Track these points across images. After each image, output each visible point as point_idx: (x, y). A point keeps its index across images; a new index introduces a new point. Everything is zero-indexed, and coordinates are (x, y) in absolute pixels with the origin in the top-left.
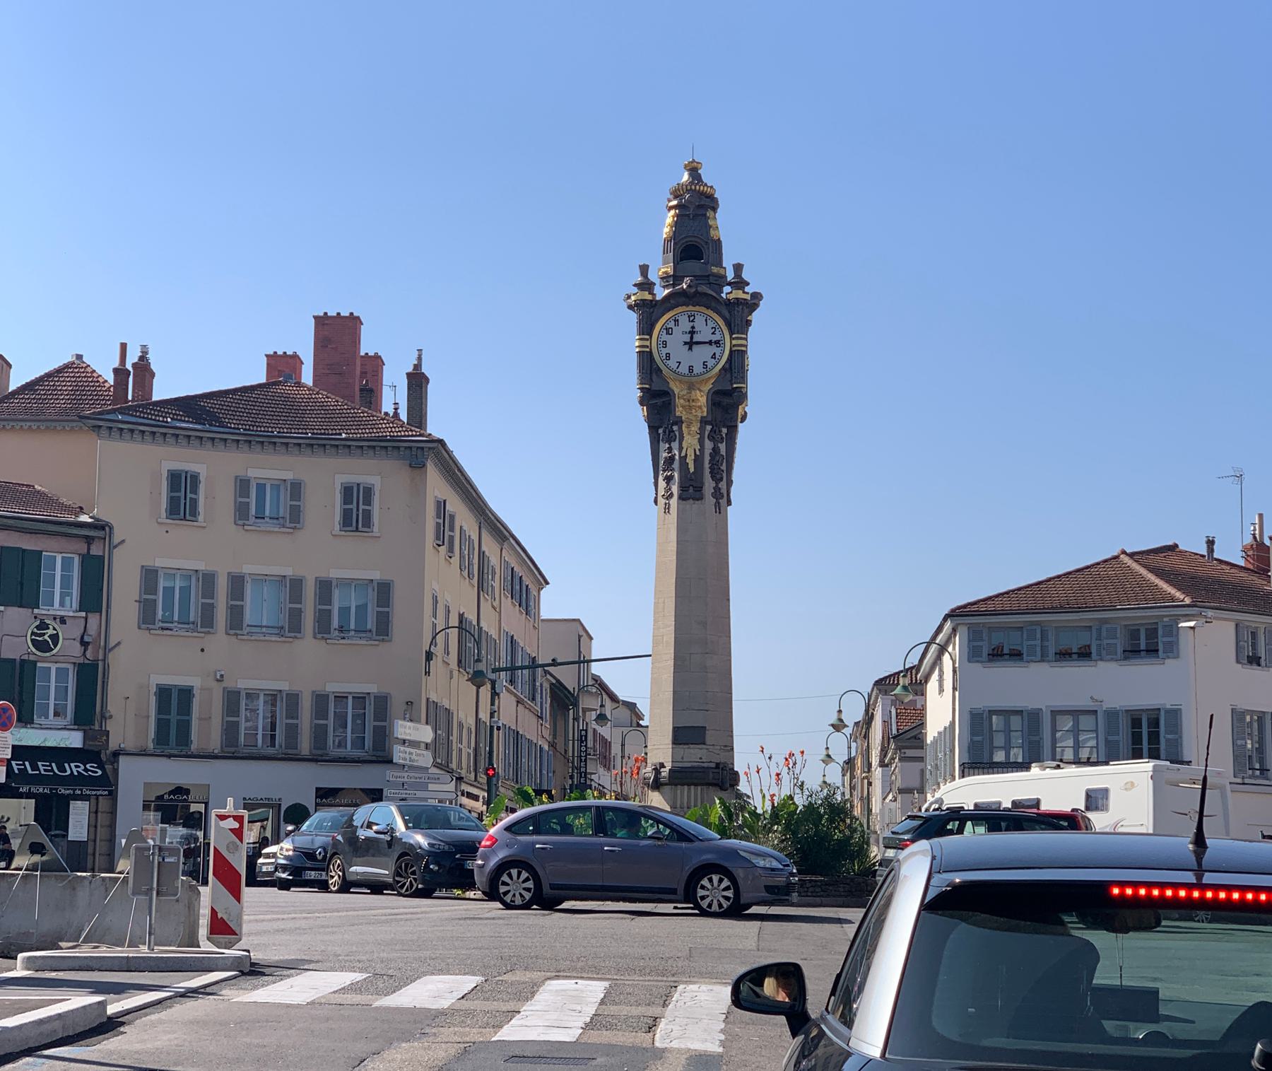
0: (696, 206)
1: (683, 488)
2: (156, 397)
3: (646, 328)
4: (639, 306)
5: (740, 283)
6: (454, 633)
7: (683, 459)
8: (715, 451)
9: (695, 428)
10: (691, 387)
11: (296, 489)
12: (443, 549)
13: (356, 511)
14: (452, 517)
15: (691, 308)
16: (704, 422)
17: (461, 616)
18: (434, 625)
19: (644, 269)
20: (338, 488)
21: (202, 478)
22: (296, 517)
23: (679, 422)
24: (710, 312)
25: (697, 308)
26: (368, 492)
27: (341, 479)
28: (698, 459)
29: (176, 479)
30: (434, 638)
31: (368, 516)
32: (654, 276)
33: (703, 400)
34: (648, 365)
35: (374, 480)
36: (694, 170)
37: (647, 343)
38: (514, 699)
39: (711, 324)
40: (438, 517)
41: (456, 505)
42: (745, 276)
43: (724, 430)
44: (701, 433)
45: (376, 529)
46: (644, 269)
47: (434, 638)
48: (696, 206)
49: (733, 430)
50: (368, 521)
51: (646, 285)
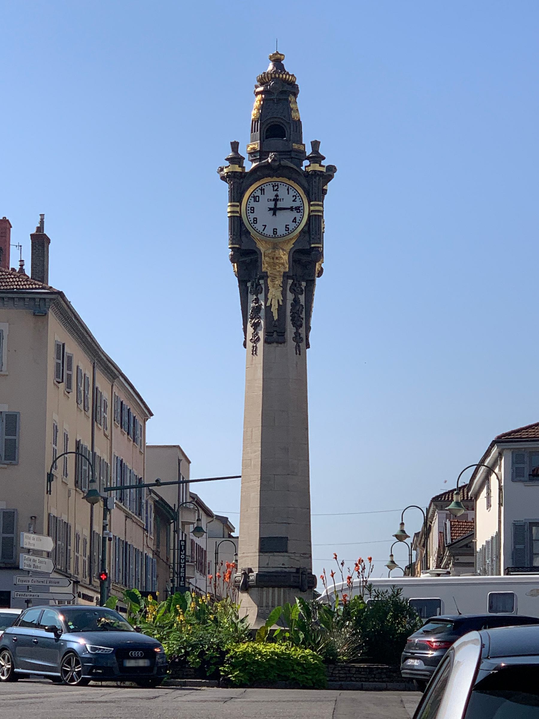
0: (279, 91)
3: (236, 196)
5: (317, 158)
6: (71, 458)
8: (296, 301)
9: (279, 282)
10: (275, 247)
12: (62, 386)
14: (70, 359)
15: (275, 179)
16: (286, 276)
17: (78, 443)
18: (55, 451)
19: (235, 146)
21: (5, 334)
23: (265, 276)
24: (291, 183)
25: (280, 179)
28: (281, 309)
32: (243, 152)
33: (285, 258)
34: (239, 229)
36: (277, 61)
37: (238, 209)
38: (123, 515)
39: (292, 193)
40: (58, 358)
41: (73, 348)
43: (304, 284)
46: (235, 146)
48: (279, 91)
49: (311, 283)
51: (236, 160)
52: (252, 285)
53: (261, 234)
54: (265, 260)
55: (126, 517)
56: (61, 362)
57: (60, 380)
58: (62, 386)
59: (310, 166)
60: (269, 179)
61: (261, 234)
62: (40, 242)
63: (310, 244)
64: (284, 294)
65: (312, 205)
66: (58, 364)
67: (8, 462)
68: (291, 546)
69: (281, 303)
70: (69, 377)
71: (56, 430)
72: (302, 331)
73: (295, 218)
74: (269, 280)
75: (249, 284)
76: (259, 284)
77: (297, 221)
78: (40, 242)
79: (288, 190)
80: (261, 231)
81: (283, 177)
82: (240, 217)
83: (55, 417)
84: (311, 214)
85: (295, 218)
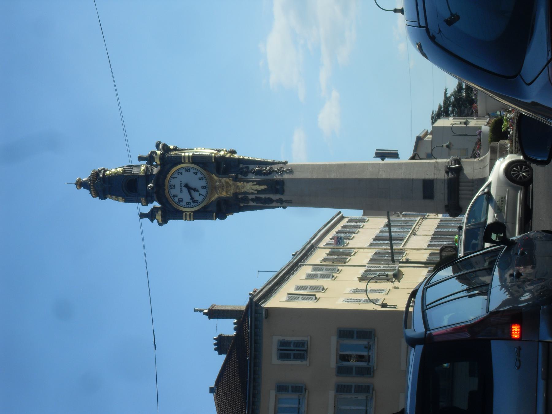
0: (104, 186)
1: (277, 192)
2: (233, 333)
3: (178, 215)
4: (164, 221)
5: (150, 159)
6: (373, 285)
7: (259, 192)
8: (253, 200)
9: (240, 184)
10: (215, 188)
11: (282, 388)
12: (318, 294)
13: (294, 351)
14: (299, 288)
15: (166, 187)
16: (235, 179)
17: (362, 279)
18: (365, 301)
19: (142, 216)
20: (280, 362)
21: (281, 338)
22: (298, 389)
23: (236, 194)
24: (169, 176)
25: (166, 183)
26: (283, 344)
27: (275, 360)
28: (259, 183)
29: (283, 356)
30: (371, 301)
31: (297, 344)
32: (146, 209)
33: (224, 180)
34: (203, 214)
35: (276, 339)
36: (80, 184)
37: (187, 161)
38: (413, 238)
39: (176, 175)
40: (298, 299)
41: (289, 286)
42: (146, 154)
43: (241, 166)
44: (244, 181)
45: (305, 339)
46: (142, 216)
47: (371, 301)
48: (104, 186)
49: (240, 161)
50: (301, 344)
51: (151, 216)
52: (242, 203)
53: (205, 197)
54: (224, 194)
55: (415, 235)
56: (301, 296)
57: (314, 297)
58: (318, 294)
59: (158, 220)
60: (166, 191)
61: (205, 197)
62: (213, 314)
63: (213, 162)
64: (248, 181)
65: (185, 161)
66: (303, 299)
67: (371, 391)
68: (428, 201)
69: (255, 183)
70: (313, 288)
71: (349, 301)
72: (275, 168)
73: (194, 173)
74: (238, 191)
75: (242, 205)
76: (242, 198)
77: (196, 171)
78: (213, 314)
79: (174, 178)
80: (203, 197)
81: (165, 182)
82: (194, 212)
83: (341, 300)
84: (191, 161)
85: (194, 173)
